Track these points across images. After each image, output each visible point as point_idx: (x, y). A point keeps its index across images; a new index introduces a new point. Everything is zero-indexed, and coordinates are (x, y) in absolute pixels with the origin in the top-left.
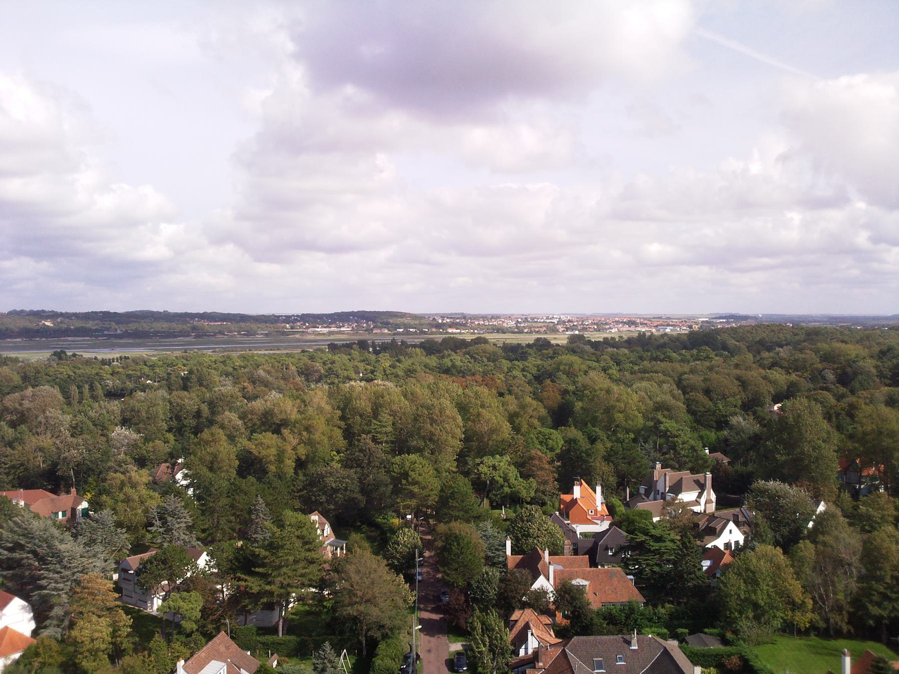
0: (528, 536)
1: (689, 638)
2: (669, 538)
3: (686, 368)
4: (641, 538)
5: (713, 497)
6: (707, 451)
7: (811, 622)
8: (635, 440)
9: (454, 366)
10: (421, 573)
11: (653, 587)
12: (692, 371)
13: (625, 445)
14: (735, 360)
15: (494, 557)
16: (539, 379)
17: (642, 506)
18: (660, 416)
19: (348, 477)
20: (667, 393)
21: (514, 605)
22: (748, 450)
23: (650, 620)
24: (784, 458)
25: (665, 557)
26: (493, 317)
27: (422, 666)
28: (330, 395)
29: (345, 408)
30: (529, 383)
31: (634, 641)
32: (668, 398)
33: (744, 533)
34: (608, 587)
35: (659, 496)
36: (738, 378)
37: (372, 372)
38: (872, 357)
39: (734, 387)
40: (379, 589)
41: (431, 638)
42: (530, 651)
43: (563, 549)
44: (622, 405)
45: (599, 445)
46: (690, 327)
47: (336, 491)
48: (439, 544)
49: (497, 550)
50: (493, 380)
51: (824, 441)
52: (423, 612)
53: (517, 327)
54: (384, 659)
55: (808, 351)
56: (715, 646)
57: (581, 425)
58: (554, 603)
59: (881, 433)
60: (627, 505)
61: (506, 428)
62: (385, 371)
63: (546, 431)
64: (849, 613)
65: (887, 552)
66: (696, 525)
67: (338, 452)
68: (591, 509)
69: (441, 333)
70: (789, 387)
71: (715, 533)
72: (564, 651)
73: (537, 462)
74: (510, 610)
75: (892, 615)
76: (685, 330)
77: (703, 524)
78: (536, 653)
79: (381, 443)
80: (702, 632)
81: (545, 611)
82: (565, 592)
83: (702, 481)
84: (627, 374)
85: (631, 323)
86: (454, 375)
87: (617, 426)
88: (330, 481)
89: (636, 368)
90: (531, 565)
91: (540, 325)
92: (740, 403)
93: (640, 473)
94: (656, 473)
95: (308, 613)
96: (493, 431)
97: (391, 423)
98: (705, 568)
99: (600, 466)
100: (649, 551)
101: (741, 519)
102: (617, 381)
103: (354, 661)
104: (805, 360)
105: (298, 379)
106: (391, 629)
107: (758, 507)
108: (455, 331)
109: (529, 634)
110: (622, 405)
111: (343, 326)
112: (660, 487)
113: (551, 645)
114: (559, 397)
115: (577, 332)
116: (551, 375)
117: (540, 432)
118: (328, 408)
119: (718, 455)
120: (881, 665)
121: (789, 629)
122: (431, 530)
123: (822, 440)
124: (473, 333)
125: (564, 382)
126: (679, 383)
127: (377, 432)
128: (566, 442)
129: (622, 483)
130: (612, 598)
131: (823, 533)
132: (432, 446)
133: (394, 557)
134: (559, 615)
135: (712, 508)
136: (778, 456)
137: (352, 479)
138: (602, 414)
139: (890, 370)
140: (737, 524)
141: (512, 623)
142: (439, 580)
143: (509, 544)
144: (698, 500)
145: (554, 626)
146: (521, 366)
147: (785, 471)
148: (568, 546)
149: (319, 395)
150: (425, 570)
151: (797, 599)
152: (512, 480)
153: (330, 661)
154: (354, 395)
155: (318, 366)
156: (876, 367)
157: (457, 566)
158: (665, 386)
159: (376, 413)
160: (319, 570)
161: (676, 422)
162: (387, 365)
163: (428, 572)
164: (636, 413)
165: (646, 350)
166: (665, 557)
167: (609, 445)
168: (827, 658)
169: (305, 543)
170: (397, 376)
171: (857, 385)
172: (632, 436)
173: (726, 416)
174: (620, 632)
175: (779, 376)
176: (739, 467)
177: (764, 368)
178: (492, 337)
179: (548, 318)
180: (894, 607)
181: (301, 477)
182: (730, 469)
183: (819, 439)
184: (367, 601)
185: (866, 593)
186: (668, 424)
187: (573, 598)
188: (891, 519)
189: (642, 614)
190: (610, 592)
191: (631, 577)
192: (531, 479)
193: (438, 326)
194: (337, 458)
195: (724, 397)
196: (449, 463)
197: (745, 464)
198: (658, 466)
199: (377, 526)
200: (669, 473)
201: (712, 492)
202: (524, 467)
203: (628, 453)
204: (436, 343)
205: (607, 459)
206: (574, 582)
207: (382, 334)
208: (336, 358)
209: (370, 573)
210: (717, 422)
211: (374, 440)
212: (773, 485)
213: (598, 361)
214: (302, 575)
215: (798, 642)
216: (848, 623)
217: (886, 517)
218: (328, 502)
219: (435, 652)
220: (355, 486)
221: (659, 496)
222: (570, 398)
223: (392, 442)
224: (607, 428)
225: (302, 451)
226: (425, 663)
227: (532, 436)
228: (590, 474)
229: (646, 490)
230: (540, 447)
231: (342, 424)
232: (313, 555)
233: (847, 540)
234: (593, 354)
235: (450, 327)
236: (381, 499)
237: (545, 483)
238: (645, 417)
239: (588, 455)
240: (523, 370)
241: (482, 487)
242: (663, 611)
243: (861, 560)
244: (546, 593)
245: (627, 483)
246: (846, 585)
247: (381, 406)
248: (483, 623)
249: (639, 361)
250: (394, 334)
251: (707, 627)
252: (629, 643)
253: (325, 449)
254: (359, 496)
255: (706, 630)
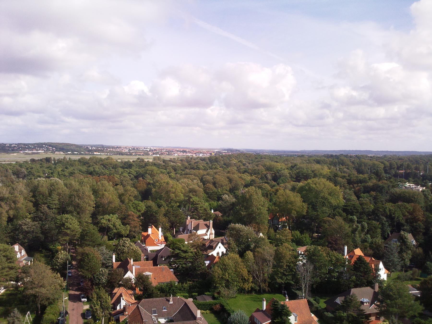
0: (123, 253)
1: (198, 297)
2: (190, 251)
3: (205, 173)
4: (177, 251)
5: (213, 232)
6: (213, 211)
7: (252, 288)
8: (179, 206)
9: (94, 171)
10: (70, 272)
11: (182, 274)
12: (208, 174)
13: (174, 208)
14: (229, 169)
15: (107, 263)
16: (137, 177)
17: (180, 237)
18: (191, 195)
19: (34, 225)
20: (195, 184)
21: (115, 285)
22: (230, 210)
23: (180, 290)
24: (245, 213)
25: (188, 260)
26: (117, 147)
27: (69, 317)
28: (27, 185)
29: (35, 191)
30: (131, 180)
31: (171, 300)
32: (197, 188)
33: (225, 248)
34: (160, 275)
35: (189, 232)
36: (228, 178)
37: (52, 173)
38: (287, 169)
39: (226, 182)
40: (47, 280)
41: (75, 304)
42: (122, 307)
43: (140, 258)
44: (174, 190)
45: (162, 209)
46: (211, 154)
47: (27, 232)
48: (79, 258)
49: (108, 260)
50: (113, 178)
51: (262, 206)
52: (71, 291)
53: (129, 152)
54: (50, 315)
55: (260, 166)
56: (209, 300)
57: (154, 199)
58: (135, 284)
59: (287, 202)
60: (174, 236)
61: (117, 202)
62: (59, 173)
63: (136, 202)
64: (269, 282)
65: (285, 255)
66: (204, 245)
67: (30, 214)
68: (156, 239)
69: (90, 155)
70: (251, 182)
71: (212, 248)
72: (138, 306)
73: (131, 217)
74: (113, 288)
75: (286, 282)
76: (208, 155)
77: (207, 244)
78: (124, 308)
79: (52, 209)
80: (204, 294)
81: (132, 288)
82: (140, 279)
83: (208, 225)
84: (178, 175)
85: (184, 151)
86: (94, 175)
87: (171, 200)
88: (25, 227)
89: (183, 172)
90: (125, 266)
91: (141, 151)
92: (228, 189)
93: (180, 221)
94: (187, 221)
95: (11, 295)
96: (110, 203)
97: (57, 199)
98: (207, 265)
99: (162, 219)
100: (181, 258)
101: (224, 241)
102: (173, 179)
103: (34, 317)
104: (259, 170)
105: (13, 177)
106: (54, 300)
107: (231, 235)
108: (98, 153)
109: (122, 299)
110: (174, 190)
111: (40, 150)
112: (189, 227)
113: (132, 304)
114: (145, 186)
115: (158, 155)
116: (143, 176)
117: (134, 203)
118: (25, 191)
119: (218, 213)
120: (276, 303)
121: (241, 291)
122: (76, 252)
123: (261, 204)
124: (107, 155)
125: (149, 179)
126: (201, 180)
127: (50, 204)
128: (146, 207)
129: (172, 227)
130: (163, 280)
131: (258, 247)
132: (78, 210)
133: (56, 265)
134: (137, 290)
135: (213, 237)
136: (242, 213)
137: (37, 227)
138: (165, 194)
139: (295, 174)
140: (223, 244)
141: (114, 294)
142: (79, 275)
143: (114, 257)
144: (207, 233)
145: (134, 294)
146: (128, 171)
147: (245, 219)
148: (143, 257)
149: (21, 186)
150: (73, 271)
151: (246, 277)
152: (118, 226)
153: (17, 318)
154: (40, 185)
155: (24, 170)
156: (289, 173)
157: (87, 268)
158: (195, 181)
159: (50, 195)
160: (15, 272)
161: (199, 198)
162: (60, 170)
163: (75, 272)
164: (180, 194)
165: (189, 165)
166: (188, 260)
167: (167, 209)
168: (259, 302)
169: (8, 259)
170: (65, 176)
171: (281, 181)
172: (178, 204)
173: (220, 195)
174: (166, 296)
175: (248, 178)
176: (225, 218)
177: (241, 173)
178: (115, 157)
179: (144, 148)
180: (287, 278)
181: (10, 226)
182: (222, 219)
183: (260, 205)
184: (41, 286)
185: (275, 273)
186: (195, 199)
187: (144, 281)
188: (290, 240)
189: (176, 287)
190: (162, 277)
191: (172, 270)
192: (128, 225)
193: (89, 151)
194: (29, 216)
195: (222, 186)
196: (87, 218)
197: (228, 216)
198: (189, 218)
199: (50, 250)
200: (193, 220)
201: (213, 229)
202: (124, 220)
203: (175, 212)
204: (86, 159)
205: (165, 215)
206: (144, 274)
207: (61, 154)
208: (33, 166)
209: (42, 272)
210: (217, 197)
211: (49, 207)
212: (238, 226)
213: (166, 169)
214: (6, 275)
215: (247, 296)
216: (268, 287)
217: (288, 240)
218: (24, 239)
219: (75, 311)
220: (39, 230)
221: (189, 232)
222: (152, 186)
223: (58, 208)
224: (167, 201)
225: (11, 213)
226: (70, 315)
227: (130, 205)
228: (157, 222)
229: (183, 229)
230: (133, 210)
231: (33, 199)
232: (12, 265)
233: (268, 250)
234: (164, 166)
235: (95, 151)
236: (52, 237)
237: (135, 227)
238: (184, 195)
239: (156, 213)
240: (129, 173)
241: (104, 230)
242: (186, 285)
243: (274, 259)
244: (131, 279)
245: (174, 226)
246: (269, 270)
247: (54, 190)
248: (98, 295)
249: (185, 169)
250: (66, 155)
251: (206, 292)
252: (169, 301)
253: (23, 211)
254: (41, 235)
255: (206, 293)
